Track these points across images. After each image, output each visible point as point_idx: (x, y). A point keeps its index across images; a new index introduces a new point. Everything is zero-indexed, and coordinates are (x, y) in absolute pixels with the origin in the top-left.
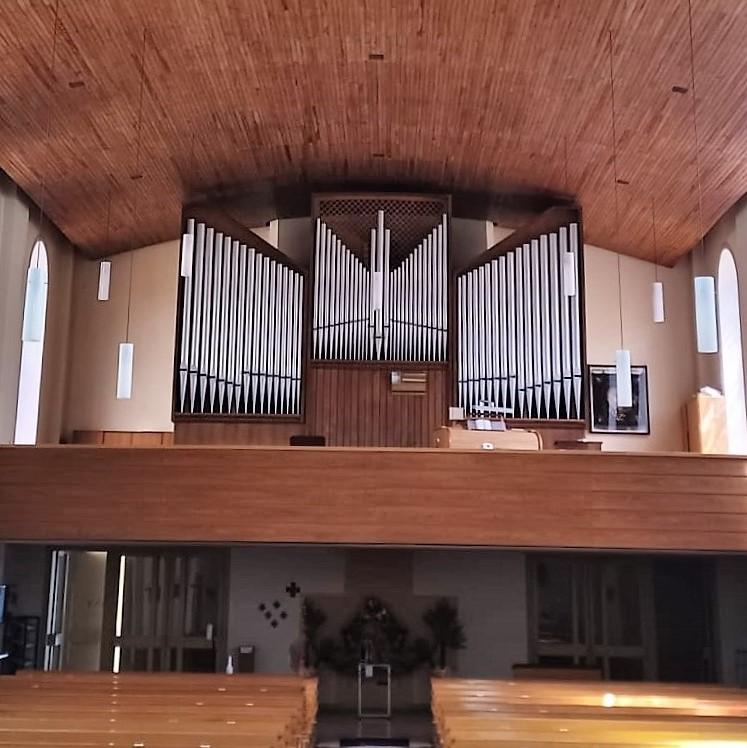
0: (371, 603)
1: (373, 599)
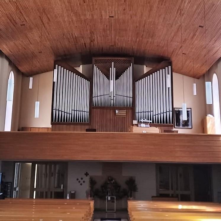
0: (110, 178)
1: (110, 177)
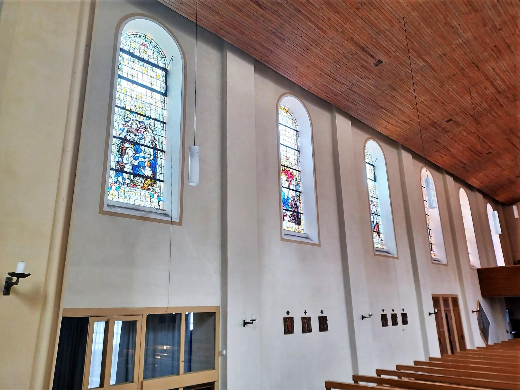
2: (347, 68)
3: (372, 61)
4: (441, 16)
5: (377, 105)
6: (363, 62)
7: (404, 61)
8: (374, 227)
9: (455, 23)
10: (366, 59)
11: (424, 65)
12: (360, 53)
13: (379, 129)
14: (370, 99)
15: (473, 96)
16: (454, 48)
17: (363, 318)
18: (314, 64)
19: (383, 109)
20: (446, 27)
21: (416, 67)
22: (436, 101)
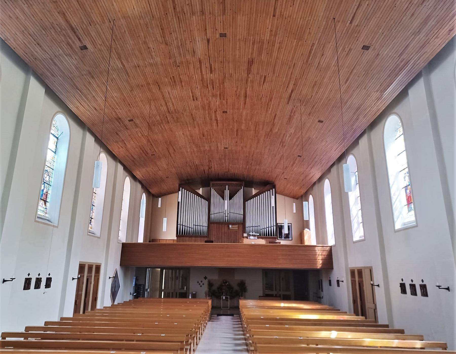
0: (224, 281)
1: (224, 280)
2: (53, 38)
3: (78, 44)
4: (142, 35)
5: (75, 85)
6: (70, 41)
7: (106, 56)
8: (43, 195)
9: (151, 46)
10: (73, 39)
11: (121, 68)
12: (69, 32)
13: (71, 106)
14: (69, 77)
15: (152, 107)
16: (147, 64)
17: (4, 281)
18: (18, 18)
19: (79, 90)
20: (144, 45)
21: (115, 67)
22: (124, 101)
